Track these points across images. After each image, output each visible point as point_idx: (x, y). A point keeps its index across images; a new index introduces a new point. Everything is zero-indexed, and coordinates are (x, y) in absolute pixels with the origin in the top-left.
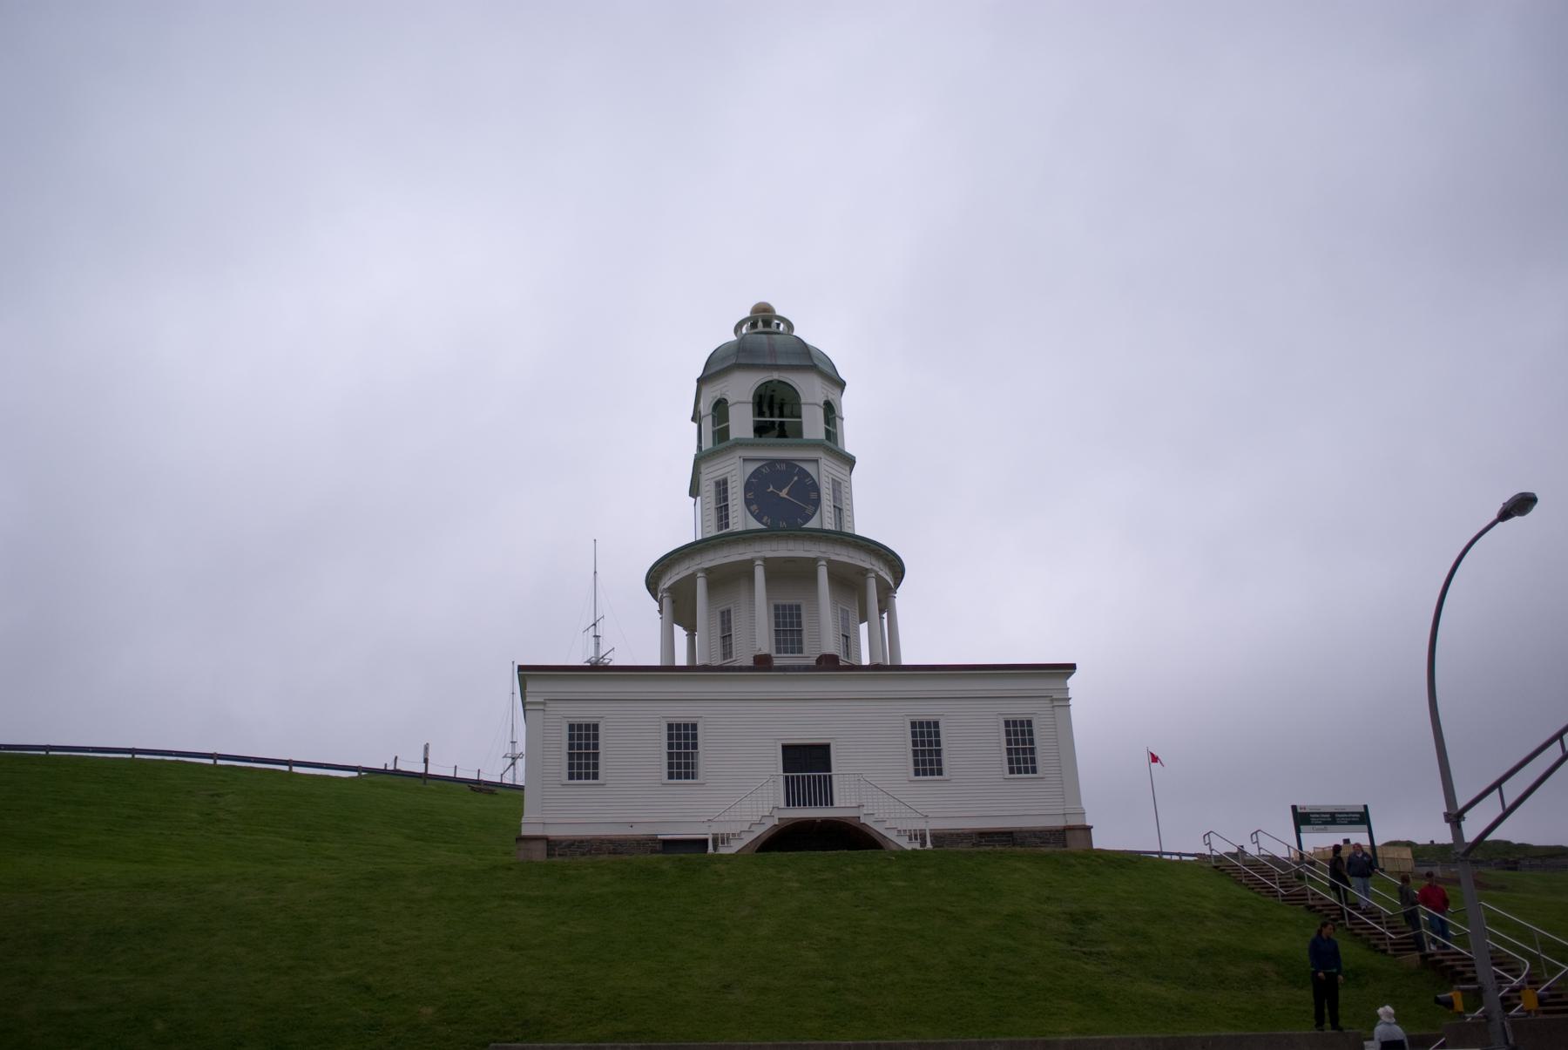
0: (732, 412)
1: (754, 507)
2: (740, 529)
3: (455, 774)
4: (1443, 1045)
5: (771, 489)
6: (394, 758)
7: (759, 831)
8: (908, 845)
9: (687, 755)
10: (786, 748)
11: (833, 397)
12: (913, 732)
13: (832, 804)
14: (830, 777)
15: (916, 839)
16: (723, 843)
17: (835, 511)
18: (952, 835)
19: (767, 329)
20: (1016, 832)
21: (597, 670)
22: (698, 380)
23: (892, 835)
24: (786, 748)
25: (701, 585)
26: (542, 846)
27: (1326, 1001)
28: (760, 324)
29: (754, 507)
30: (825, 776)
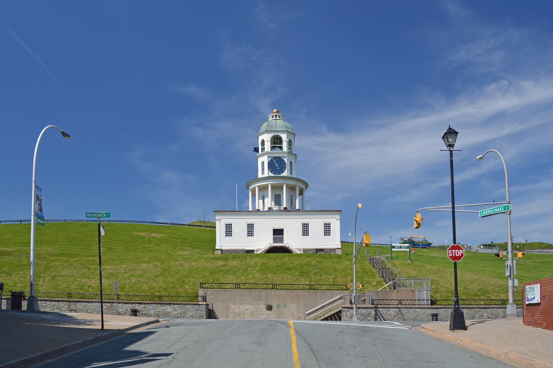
0: (266, 143)
1: (270, 169)
4: (258, 250)
5: (278, 168)
6: (341, 210)
7: (266, 248)
8: (299, 252)
9: (252, 231)
10: (274, 230)
19: (279, 119)
23: (294, 250)
24: (274, 230)
25: (270, 187)
27: (379, 290)
28: (274, 116)
29: (270, 169)
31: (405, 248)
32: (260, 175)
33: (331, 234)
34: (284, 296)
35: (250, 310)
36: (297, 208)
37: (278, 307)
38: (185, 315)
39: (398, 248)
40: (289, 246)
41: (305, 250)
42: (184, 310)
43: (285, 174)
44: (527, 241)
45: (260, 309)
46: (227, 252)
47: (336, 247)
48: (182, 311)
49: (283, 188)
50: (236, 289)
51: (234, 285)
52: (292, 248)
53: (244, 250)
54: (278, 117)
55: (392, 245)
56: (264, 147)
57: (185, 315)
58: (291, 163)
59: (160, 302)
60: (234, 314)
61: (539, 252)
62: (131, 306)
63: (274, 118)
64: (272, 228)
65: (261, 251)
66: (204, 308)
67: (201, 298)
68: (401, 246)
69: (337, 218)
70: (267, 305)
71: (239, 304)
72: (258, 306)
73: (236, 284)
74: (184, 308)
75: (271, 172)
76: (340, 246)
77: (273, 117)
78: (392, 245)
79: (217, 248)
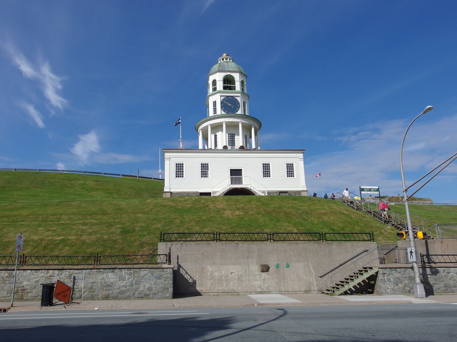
4: (215, 192)
7: (224, 190)
8: (263, 195)
19: (226, 61)
20: (289, 192)
23: (257, 192)
28: (225, 59)
29: (223, 108)
30: (241, 177)
31: (374, 191)
32: (211, 114)
33: (294, 175)
34: (285, 251)
35: (237, 273)
36: (254, 147)
37: (278, 266)
38: (137, 286)
39: (368, 191)
40: (252, 188)
41: (269, 193)
42: (136, 279)
43: (240, 112)
44: (399, 195)
45: (252, 272)
47: (301, 189)
48: (133, 281)
49: (238, 126)
50: (215, 242)
51: (368, 235)
52: (255, 190)
53: (197, 192)
54: (228, 59)
55: (361, 188)
56: (216, 87)
57: (137, 286)
58: (244, 103)
59: (98, 267)
60: (212, 281)
61: (418, 203)
62: (46, 275)
63: (225, 60)
66: (169, 274)
67: (166, 257)
68: (370, 189)
69: (298, 158)
70: (262, 266)
71: (220, 264)
72: (248, 267)
73: (370, 234)
74: (136, 275)
75: (224, 111)
76: (306, 188)
77: (223, 60)
78: (361, 188)
79: (165, 190)
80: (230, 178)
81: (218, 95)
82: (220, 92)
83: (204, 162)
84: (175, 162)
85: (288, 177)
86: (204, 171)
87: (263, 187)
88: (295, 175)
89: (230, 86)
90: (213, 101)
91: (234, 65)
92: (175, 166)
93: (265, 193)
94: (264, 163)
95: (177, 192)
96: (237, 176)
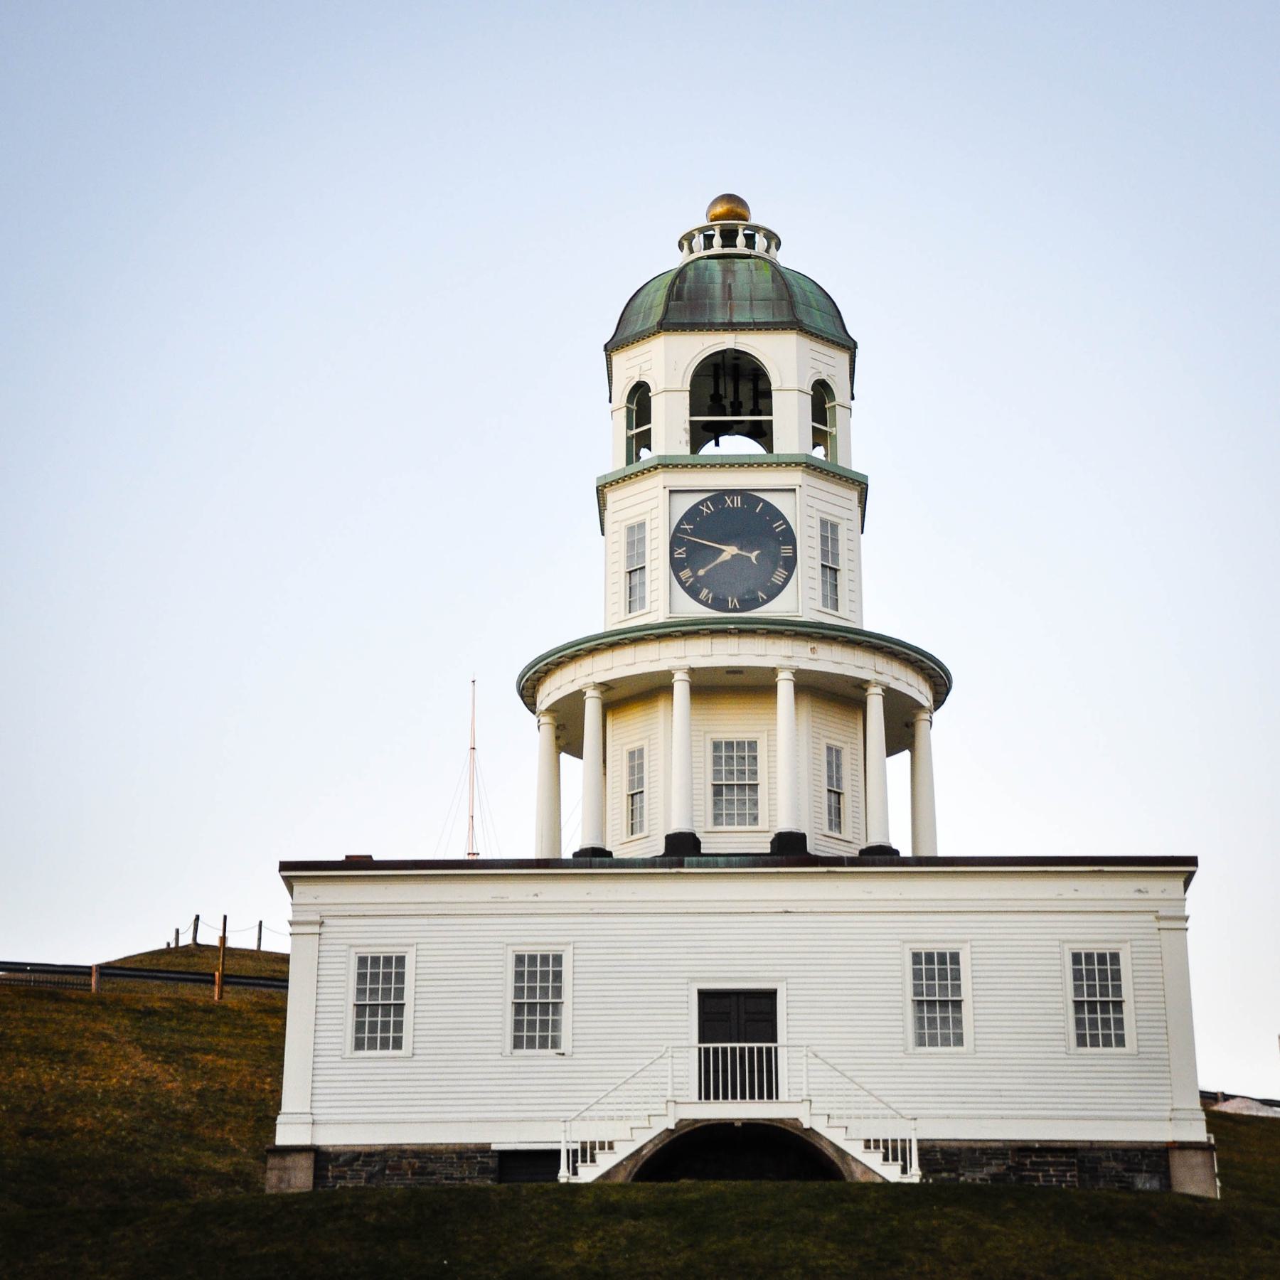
1: (685, 574)
2: (661, 620)
3: (259, 945)
4: (586, 1153)
8: (892, 1173)
10: (704, 995)
11: (832, 371)
12: (958, 978)
13: (777, 1098)
14: (776, 1048)
15: (895, 1159)
16: (584, 1161)
17: (824, 574)
18: (973, 1150)
19: (727, 251)
20: (1083, 1149)
21: (358, 865)
22: (606, 347)
23: (855, 1149)
24: (704, 995)
26: (306, 1162)
28: (717, 241)
30: (769, 1050)
40: (820, 1126)
46: (356, 1166)
52: (834, 1135)
53: (484, 1150)
56: (650, 429)
64: (693, 979)
65: (606, 1162)
69: (1162, 913)
79: (286, 1135)
80: (697, 1050)
81: (658, 483)
82: (666, 464)
83: (524, 948)
84: (510, 949)
85: (1082, 1050)
86: (532, 1006)
87: (885, 1117)
88: (1129, 1031)
89: (739, 414)
90: (630, 522)
91: (770, 285)
92: (1069, 965)
93: (904, 1159)
94: (924, 948)
95: (359, 1149)
96: (755, 1045)
